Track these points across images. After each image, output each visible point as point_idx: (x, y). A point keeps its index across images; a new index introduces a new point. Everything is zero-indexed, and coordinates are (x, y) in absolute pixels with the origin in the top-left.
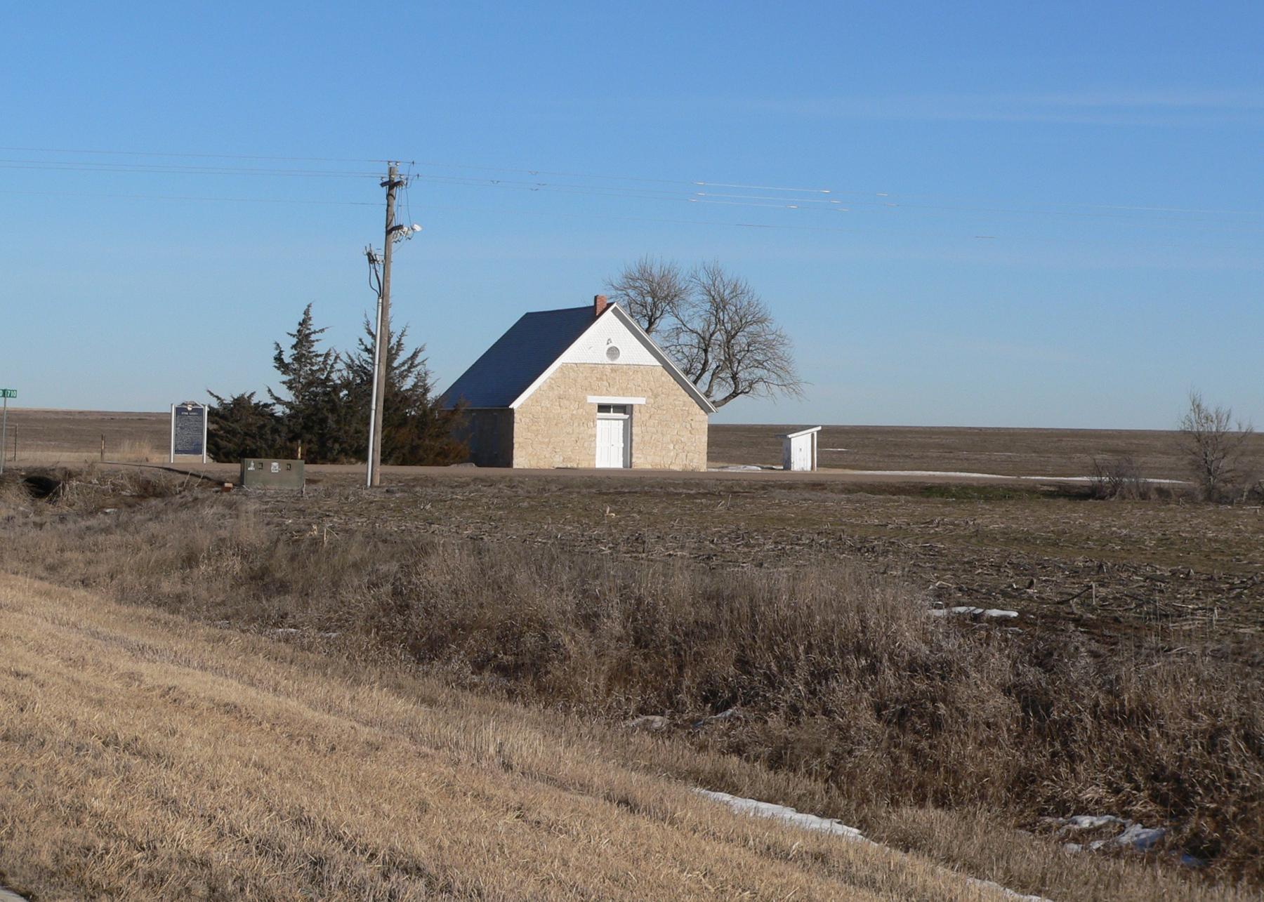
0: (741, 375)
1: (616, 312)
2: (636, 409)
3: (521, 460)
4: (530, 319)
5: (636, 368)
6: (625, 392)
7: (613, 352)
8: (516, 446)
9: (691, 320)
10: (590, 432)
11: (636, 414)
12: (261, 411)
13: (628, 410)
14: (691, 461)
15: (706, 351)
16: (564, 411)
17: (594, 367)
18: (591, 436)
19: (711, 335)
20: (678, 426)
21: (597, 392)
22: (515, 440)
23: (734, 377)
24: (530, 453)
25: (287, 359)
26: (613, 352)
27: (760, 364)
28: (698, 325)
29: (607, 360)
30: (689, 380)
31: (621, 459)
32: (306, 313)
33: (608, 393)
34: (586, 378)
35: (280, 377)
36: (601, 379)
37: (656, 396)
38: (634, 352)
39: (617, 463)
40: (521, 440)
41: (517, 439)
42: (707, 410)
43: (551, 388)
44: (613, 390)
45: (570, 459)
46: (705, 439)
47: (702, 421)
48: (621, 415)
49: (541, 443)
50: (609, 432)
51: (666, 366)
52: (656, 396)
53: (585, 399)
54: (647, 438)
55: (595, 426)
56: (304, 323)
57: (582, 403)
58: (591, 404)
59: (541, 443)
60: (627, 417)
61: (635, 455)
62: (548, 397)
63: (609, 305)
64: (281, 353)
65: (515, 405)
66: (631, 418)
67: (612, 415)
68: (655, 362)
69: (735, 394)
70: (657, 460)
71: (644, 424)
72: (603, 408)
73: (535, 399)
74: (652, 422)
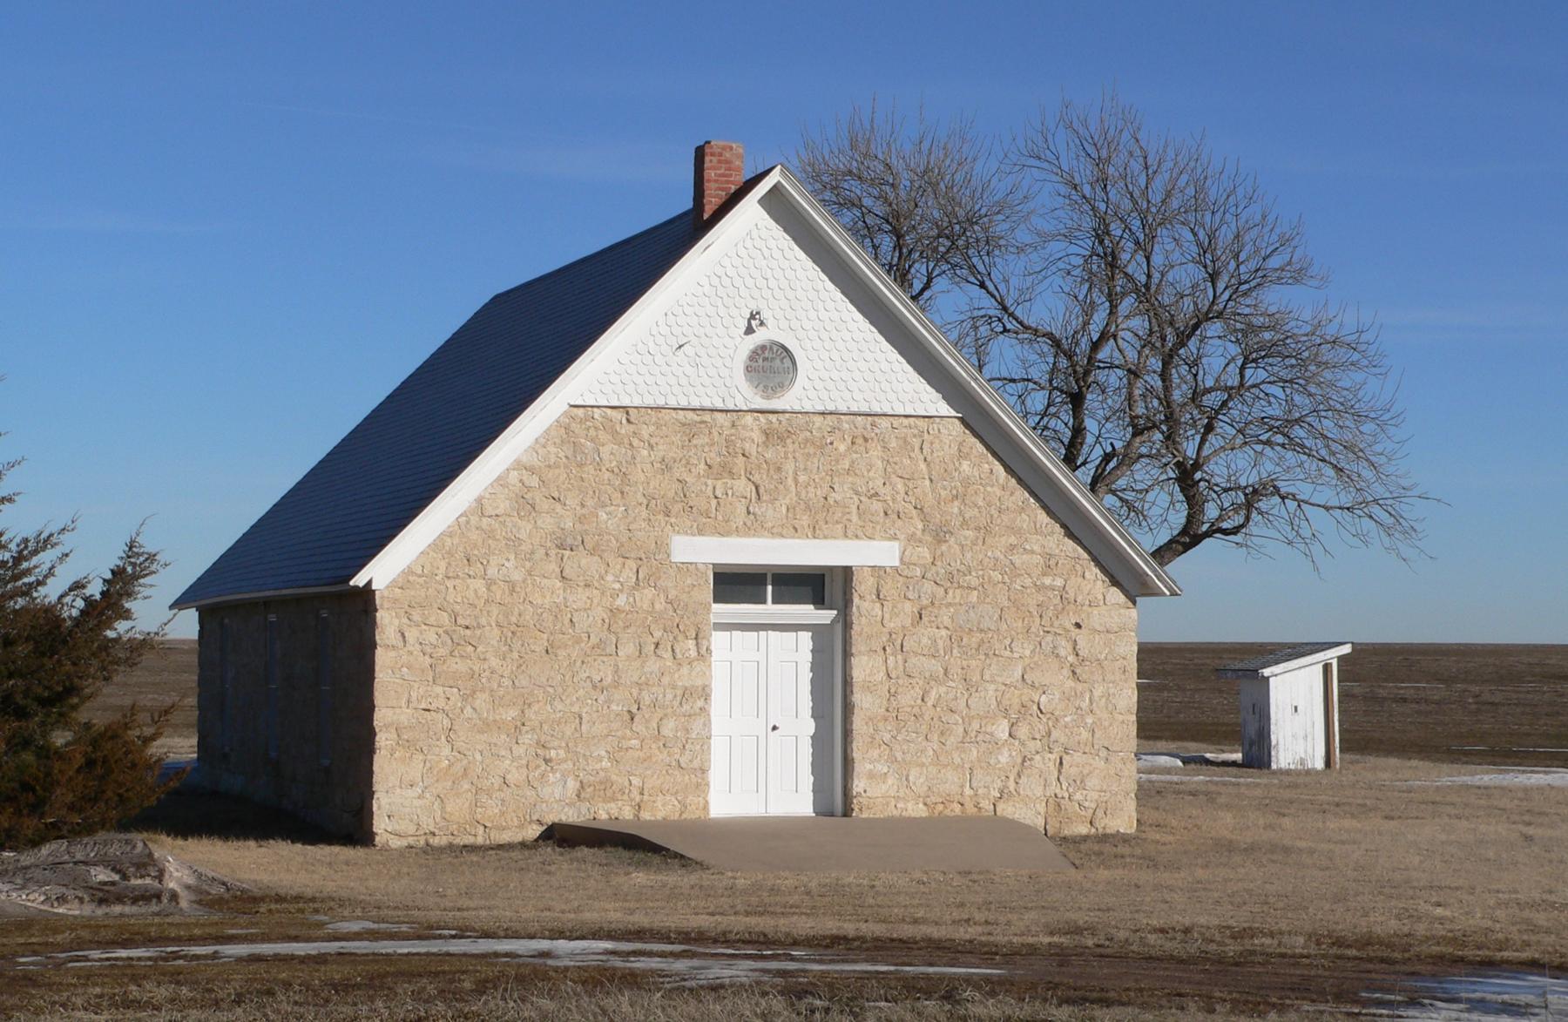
0: (1218, 469)
1: (777, 204)
2: (863, 587)
3: (407, 796)
4: (497, 299)
5: (866, 425)
7: (771, 364)
8: (383, 740)
9: (1026, 298)
10: (685, 677)
11: (864, 606)
13: (833, 589)
14: (1080, 782)
15: (1077, 400)
16: (579, 597)
18: (687, 694)
19: (1095, 346)
21: (712, 523)
22: (381, 717)
23: (1186, 477)
24: (451, 761)
26: (771, 364)
27: (1282, 430)
28: (1051, 308)
29: (746, 395)
30: (1073, 485)
31: (807, 780)
33: (754, 526)
34: (666, 466)
36: (727, 471)
37: (940, 535)
38: (851, 364)
39: (793, 799)
40: (405, 716)
41: (392, 708)
42: (1132, 585)
43: (525, 505)
44: (771, 513)
45: (606, 789)
46: (1128, 697)
47: (1116, 628)
50: (757, 678)
51: (976, 420)
52: (940, 535)
53: (662, 546)
54: (908, 699)
55: (704, 655)
57: (650, 564)
58: (686, 568)
59: (487, 726)
60: (826, 616)
61: (861, 767)
62: (514, 543)
65: (381, 572)
67: (769, 610)
68: (931, 402)
69: (1188, 538)
70: (951, 782)
71: (895, 644)
72: (735, 584)
73: (457, 551)
74: (925, 635)
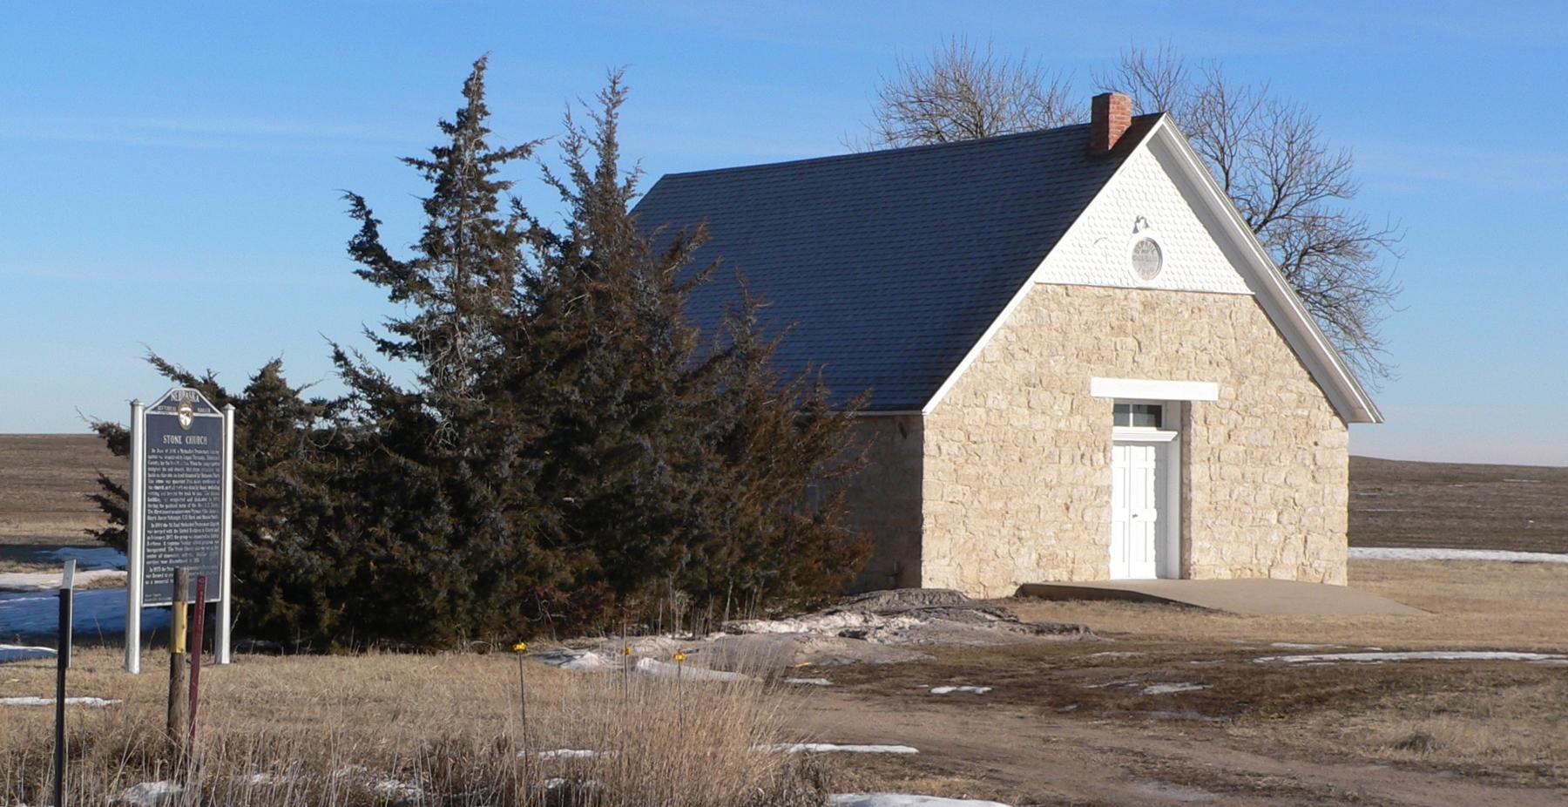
2: (1197, 414)
4: (666, 177)
6: (1173, 367)
7: (1148, 254)
8: (928, 524)
11: (1197, 427)
12: (118, 429)
16: (1039, 421)
17: (1108, 294)
20: (1286, 460)
22: (928, 507)
25: (401, 242)
26: (1148, 254)
32: (472, 88)
33: (1137, 370)
34: (1088, 328)
35: (379, 308)
37: (1241, 378)
41: (932, 505)
45: (1051, 559)
46: (1343, 495)
47: (1338, 444)
48: (1151, 433)
49: (987, 514)
52: (1241, 378)
53: (1086, 385)
54: (1222, 495)
56: (468, 122)
57: (1079, 400)
58: (1098, 401)
59: (987, 514)
60: (1168, 436)
62: (1002, 381)
63: (1142, 124)
64: (370, 227)
66: (1184, 442)
70: (1245, 554)
72: (1122, 410)
